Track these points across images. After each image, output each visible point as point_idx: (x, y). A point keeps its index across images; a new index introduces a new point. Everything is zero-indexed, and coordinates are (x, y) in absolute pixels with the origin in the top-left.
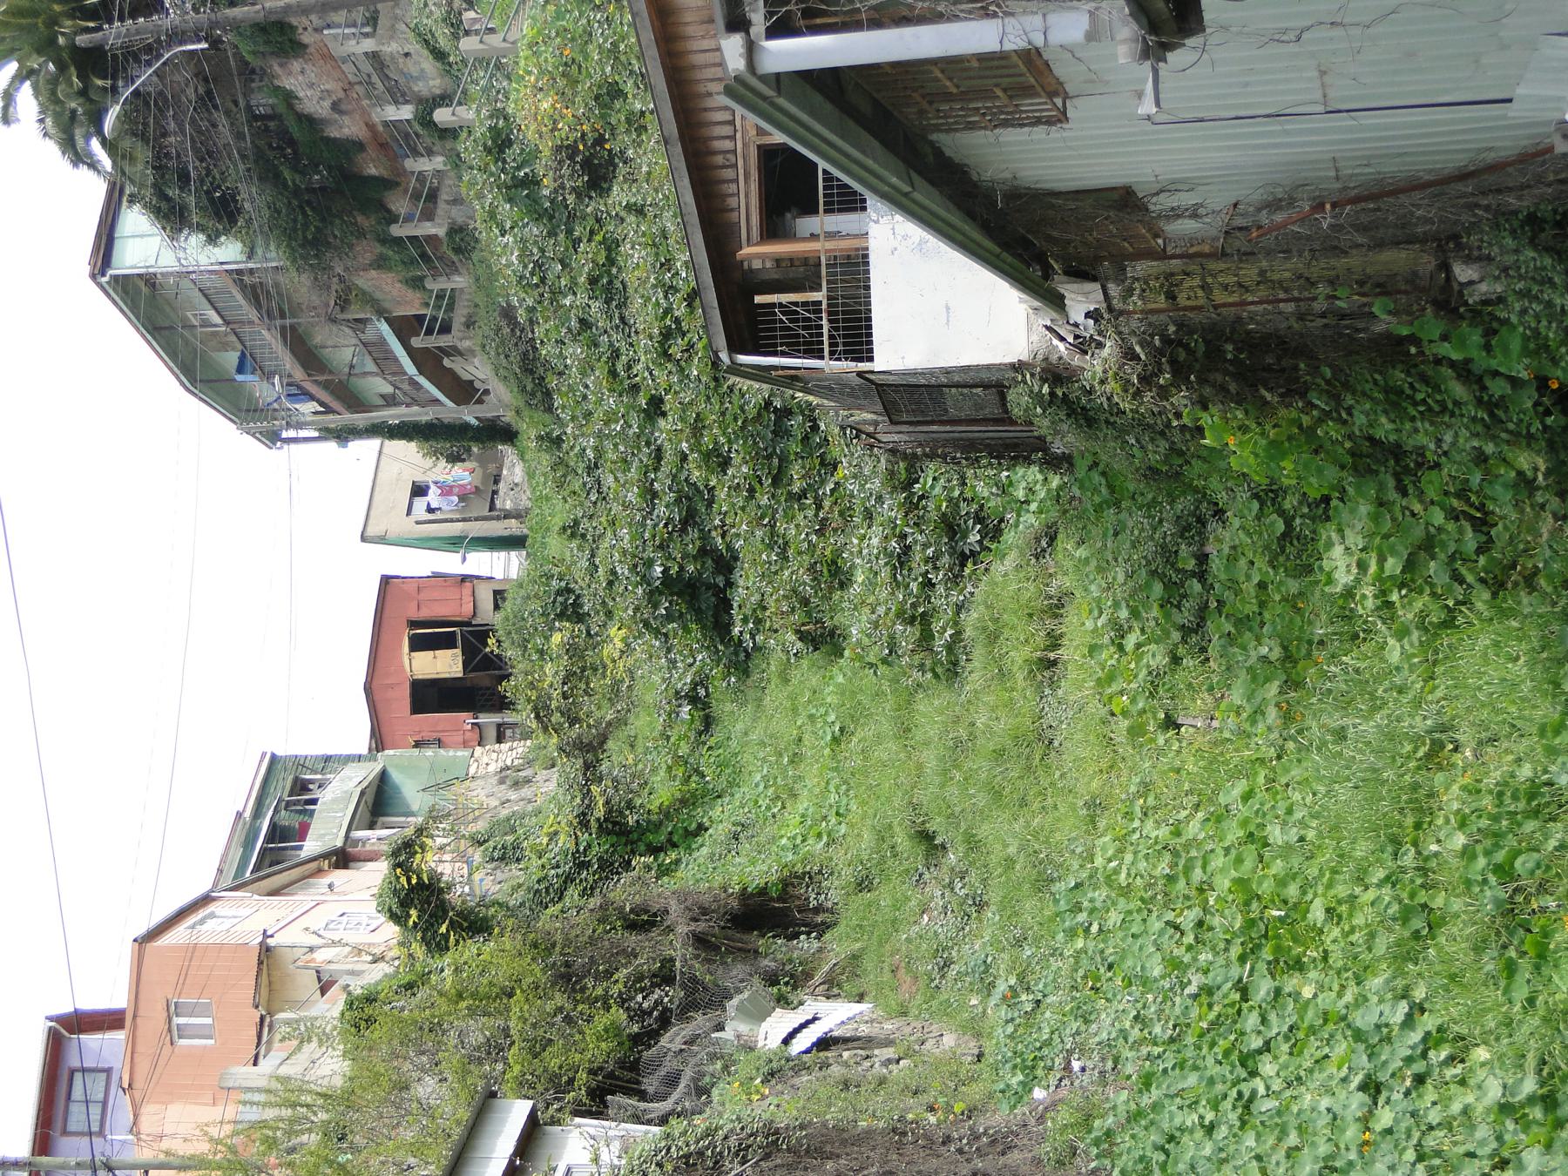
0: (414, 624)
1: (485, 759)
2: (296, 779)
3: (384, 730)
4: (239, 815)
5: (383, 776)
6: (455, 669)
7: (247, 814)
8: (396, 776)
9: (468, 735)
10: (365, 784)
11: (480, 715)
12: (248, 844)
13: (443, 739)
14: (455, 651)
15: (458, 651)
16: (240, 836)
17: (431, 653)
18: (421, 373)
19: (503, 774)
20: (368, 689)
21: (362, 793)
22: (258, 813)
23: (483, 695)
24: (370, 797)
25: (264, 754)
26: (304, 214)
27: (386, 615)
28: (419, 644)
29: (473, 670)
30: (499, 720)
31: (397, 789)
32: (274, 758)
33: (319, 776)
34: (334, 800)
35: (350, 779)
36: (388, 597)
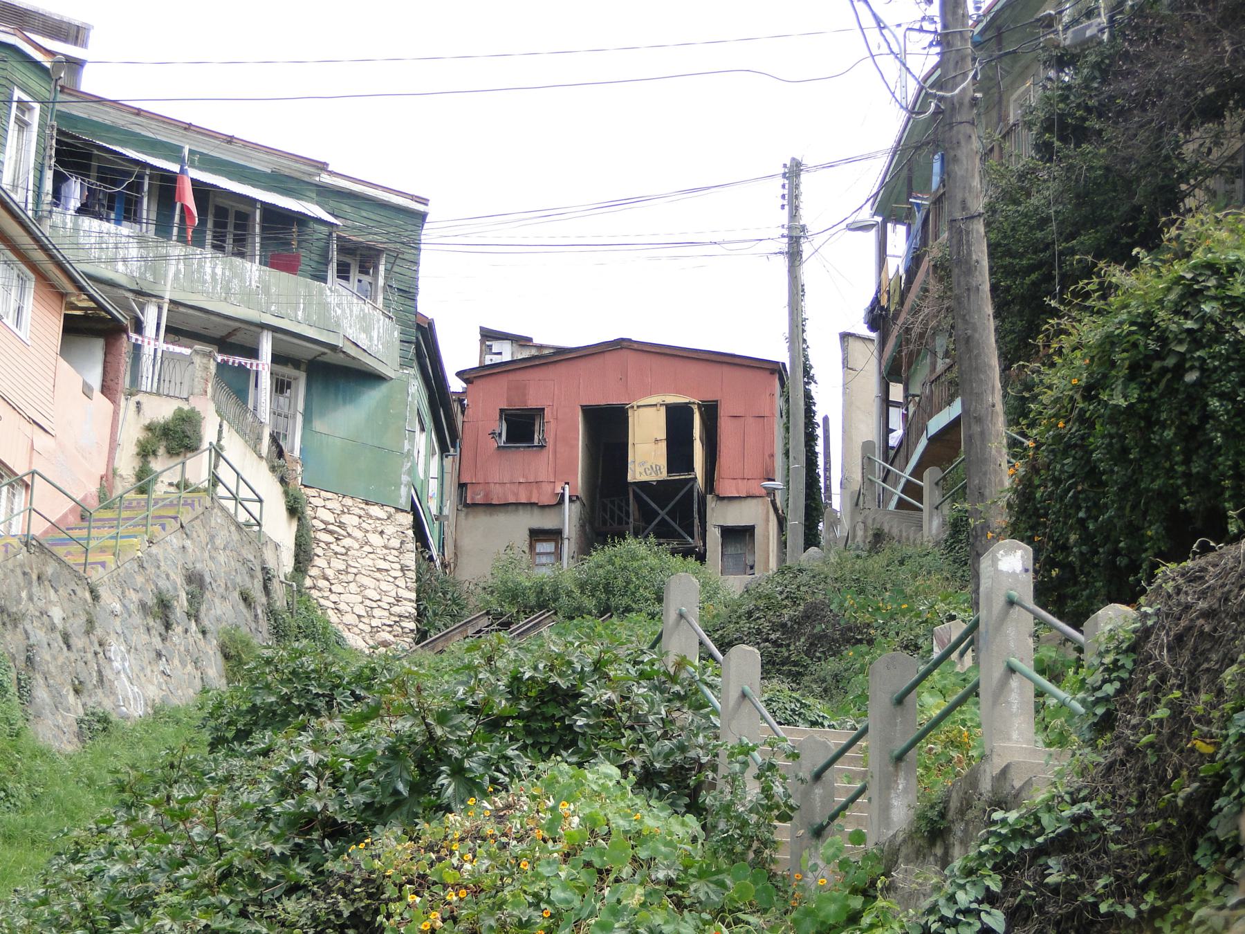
0: (710, 412)
1: (390, 530)
2: (379, 252)
3: (562, 369)
4: (322, 167)
5: (371, 378)
6: (638, 470)
7: (326, 179)
8: (372, 397)
9: (547, 488)
10: (352, 351)
11: (577, 507)
12: (278, 182)
13: (545, 451)
14: (664, 470)
15: (663, 475)
16: (288, 168)
17: (662, 435)
18: (932, 440)
19: (259, 575)
20: (620, 345)
21: (334, 348)
22: (327, 194)
23: (620, 509)
24: (331, 358)
25: (424, 202)
26: (1031, 269)
27: (726, 370)
28: (678, 419)
29: (636, 496)
30: (566, 534)
31: (350, 398)
32: (423, 216)
33: (381, 282)
34: (325, 306)
35: (366, 330)
36: (749, 374)
